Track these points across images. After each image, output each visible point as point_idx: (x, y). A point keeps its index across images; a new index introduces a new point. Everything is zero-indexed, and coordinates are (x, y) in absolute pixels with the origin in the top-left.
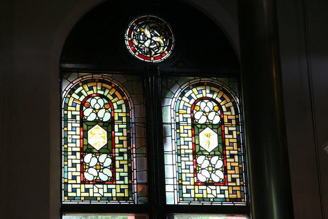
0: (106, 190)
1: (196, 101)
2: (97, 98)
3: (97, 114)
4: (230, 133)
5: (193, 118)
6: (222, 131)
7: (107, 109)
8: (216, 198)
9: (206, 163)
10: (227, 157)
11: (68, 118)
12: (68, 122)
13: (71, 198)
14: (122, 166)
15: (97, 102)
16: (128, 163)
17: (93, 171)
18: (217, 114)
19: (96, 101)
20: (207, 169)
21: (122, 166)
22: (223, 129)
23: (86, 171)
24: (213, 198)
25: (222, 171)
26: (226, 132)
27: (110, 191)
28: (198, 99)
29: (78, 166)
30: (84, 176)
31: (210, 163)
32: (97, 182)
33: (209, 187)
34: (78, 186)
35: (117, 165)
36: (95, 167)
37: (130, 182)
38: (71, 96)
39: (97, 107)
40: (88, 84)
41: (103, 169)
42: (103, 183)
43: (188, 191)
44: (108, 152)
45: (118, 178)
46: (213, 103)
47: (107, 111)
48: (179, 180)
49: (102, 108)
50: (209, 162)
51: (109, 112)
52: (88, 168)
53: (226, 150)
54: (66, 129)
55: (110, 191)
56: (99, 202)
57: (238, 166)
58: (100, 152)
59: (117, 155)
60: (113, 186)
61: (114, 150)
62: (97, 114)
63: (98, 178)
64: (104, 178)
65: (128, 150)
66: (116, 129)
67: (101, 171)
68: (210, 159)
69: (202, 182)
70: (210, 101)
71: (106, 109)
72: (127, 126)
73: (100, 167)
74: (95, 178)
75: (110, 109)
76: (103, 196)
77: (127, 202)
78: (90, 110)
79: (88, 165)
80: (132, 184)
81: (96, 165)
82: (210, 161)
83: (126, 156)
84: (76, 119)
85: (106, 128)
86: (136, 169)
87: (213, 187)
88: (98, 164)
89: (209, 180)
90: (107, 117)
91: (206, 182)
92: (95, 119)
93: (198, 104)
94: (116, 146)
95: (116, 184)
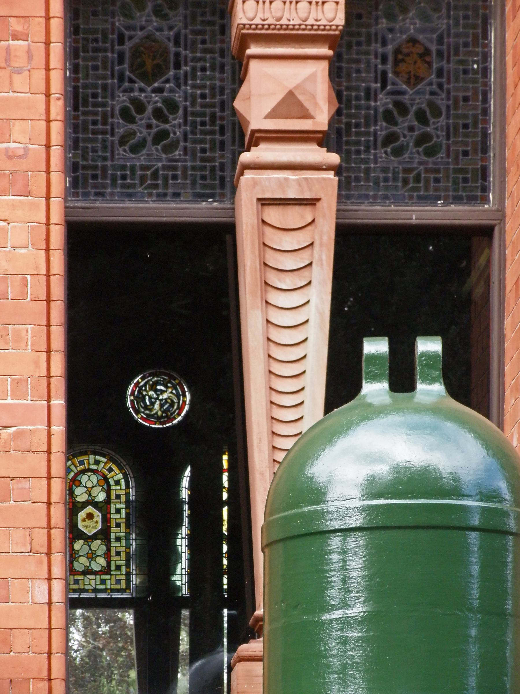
1: (76, 474)
4: (118, 511)
10: (112, 540)
15: (89, 479)
17: (83, 560)
21: (118, 553)
27: (103, 582)
28: (79, 472)
32: (87, 572)
35: (113, 553)
36: (86, 556)
42: (95, 573)
43: (118, 582)
50: (92, 547)
55: (103, 582)
58: (94, 537)
60: (108, 577)
64: (95, 567)
66: (113, 511)
67: (94, 559)
68: (90, 543)
73: (92, 556)
74: (86, 568)
75: (105, 487)
82: (89, 546)
83: (124, 542)
87: (92, 577)
88: (90, 552)
90: (101, 497)
91: (84, 571)
92: (87, 500)
93: (78, 478)
95: (111, 575)
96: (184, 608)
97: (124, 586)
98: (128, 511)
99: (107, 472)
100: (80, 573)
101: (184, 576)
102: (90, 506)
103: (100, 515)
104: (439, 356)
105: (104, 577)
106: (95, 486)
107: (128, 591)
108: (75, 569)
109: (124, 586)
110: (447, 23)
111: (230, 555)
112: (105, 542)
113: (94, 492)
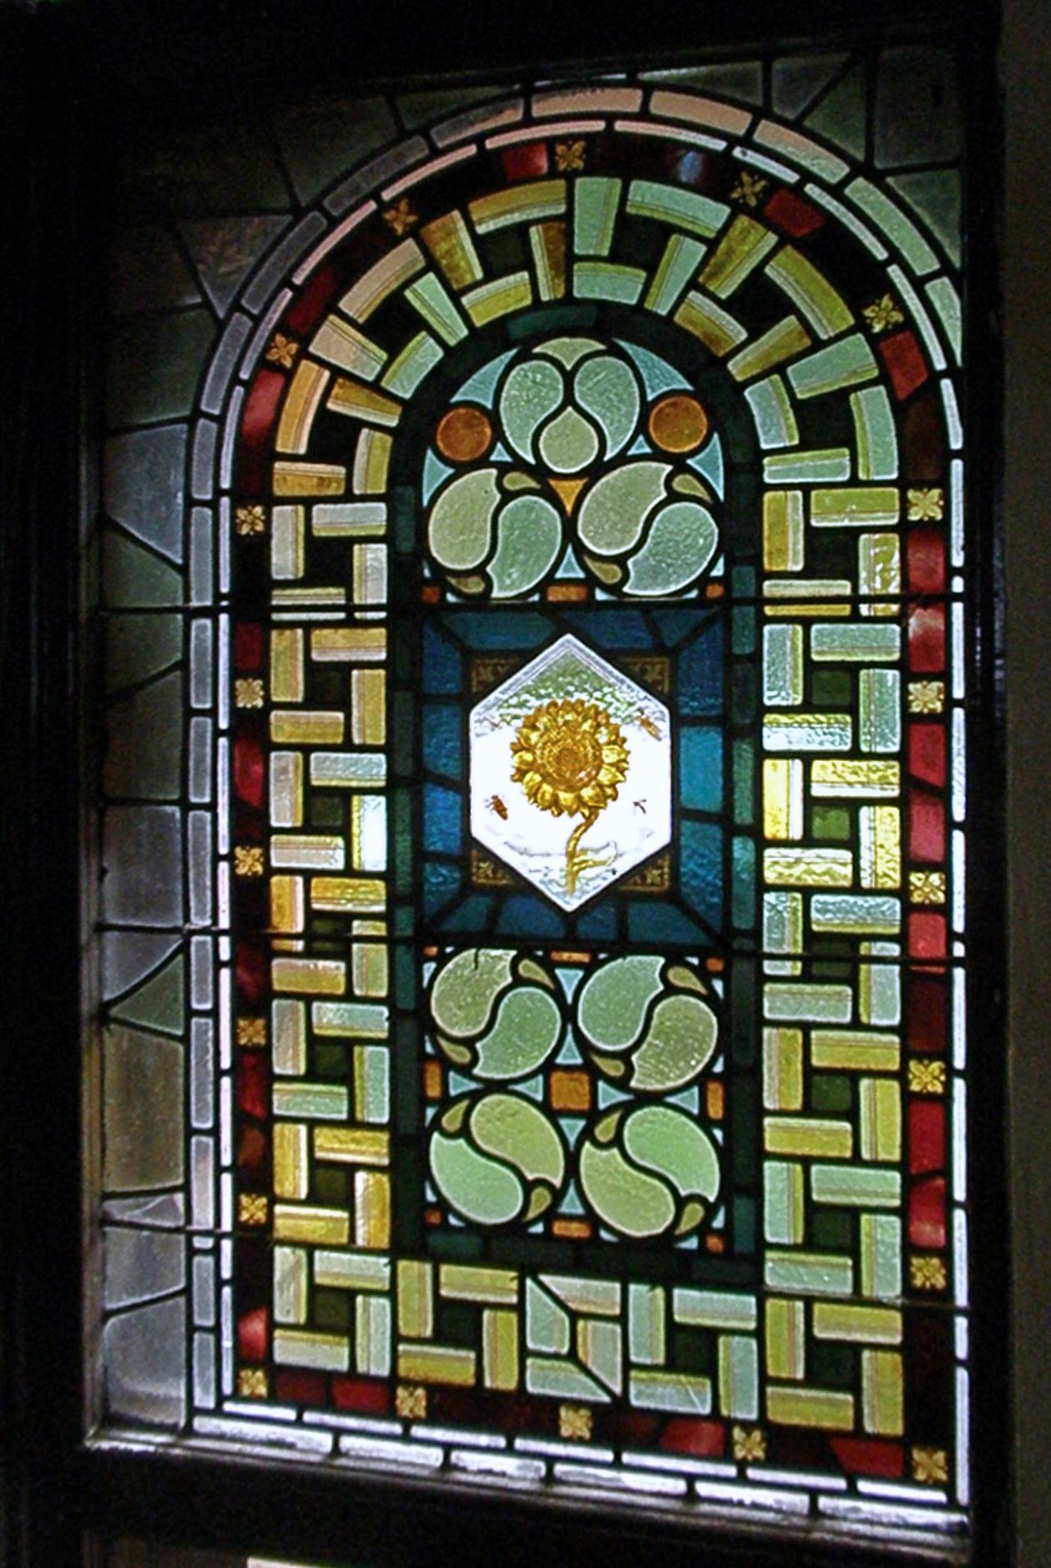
9: (360, 1020)
15: (569, 400)
18: (681, 484)
22: (743, 648)
23: (451, 1120)
25: (704, 1121)
38: (303, 354)
40: (477, 209)
44: (689, 934)
52: (627, 1109)
54: (926, 696)
69: (472, 1226)
75: (712, 465)
79: (614, 1069)
81: (548, 1068)
85: (657, 669)
87: (600, 1293)
89: (550, 1215)
91: (517, 1226)
93: (475, 389)
95: (754, 1285)
96: (476, 197)
99: (794, 944)
102: (569, 637)
103: (666, 712)
104: (339, 724)
106: (622, 459)
107: (927, 1461)
108: (443, 1206)
110: (871, 327)
111: (975, 653)
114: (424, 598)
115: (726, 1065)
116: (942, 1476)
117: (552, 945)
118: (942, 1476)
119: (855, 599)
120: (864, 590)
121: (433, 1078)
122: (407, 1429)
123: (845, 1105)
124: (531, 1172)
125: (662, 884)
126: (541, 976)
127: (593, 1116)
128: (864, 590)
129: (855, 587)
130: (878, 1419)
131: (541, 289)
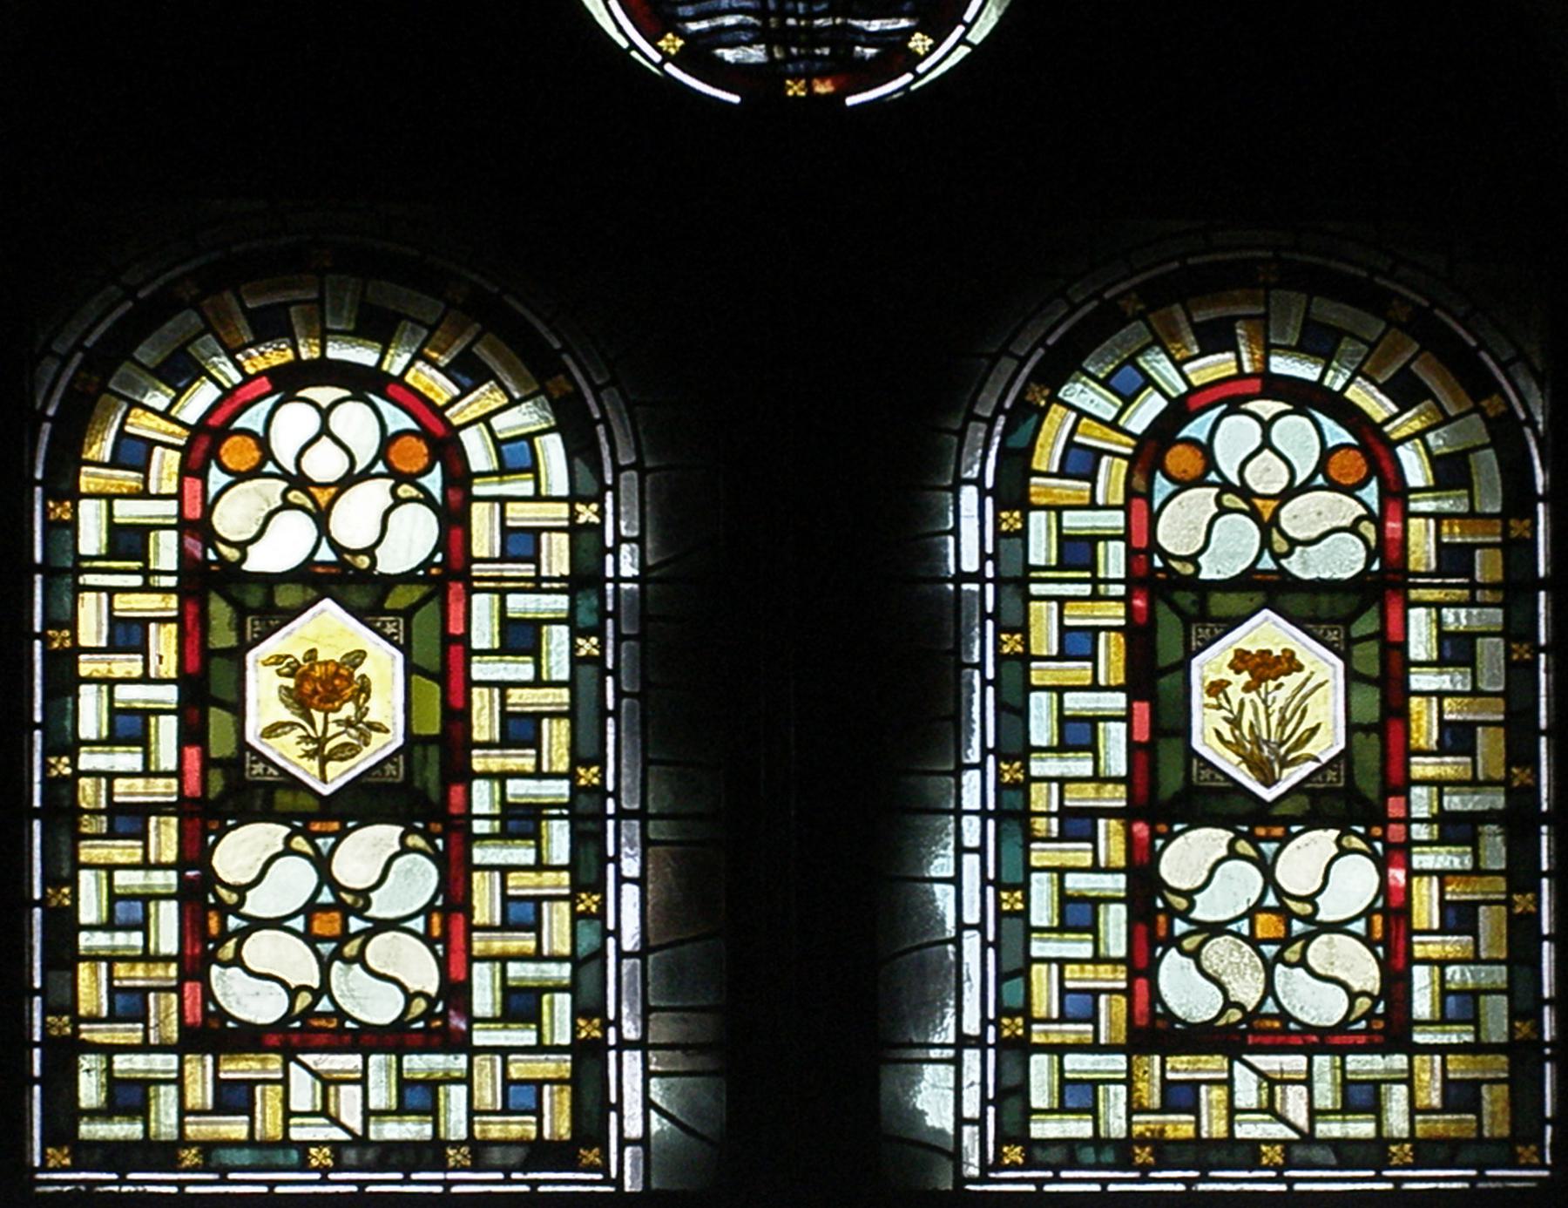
0: (1326, 1095)
2: (1267, 408)
3: (321, 518)
5: (1143, 550)
6: (447, 639)
7: (411, 479)
8: (1308, 1138)
11: (1033, 560)
12: (1414, 594)
13: (1055, 1155)
14: (1458, 918)
16: (577, 887)
19: (312, 421)
20: (298, 924)
24: (1286, 1144)
26: (484, 633)
29: (1115, 921)
30: (208, 995)
31: (1270, 880)
33: (308, 1059)
34: (164, 1063)
35: (485, 903)
37: (589, 1030)
39: (325, 464)
41: (368, 935)
45: (485, 999)
46: (385, 407)
47: (406, 490)
48: (1001, 1010)
49: (366, 475)
50: (1281, 875)
51: (428, 500)
53: (470, 776)
56: (324, 1181)
57: (1509, 903)
59: (1420, 832)
61: (457, 792)
62: (321, 518)
63: (324, 1005)
65: (574, 789)
67: (351, 949)
68: (1269, 848)
70: (1299, 410)
71: (399, 477)
72: (1507, 618)
74: (304, 1000)
75: (434, 482)
76: (1308, 1138)
77: (1378, 1178)
78: (1202, 500)
80: (600, 1047)
83: (559, 839)
84: (1093, 567)
86: (981, 927)
92: (310, 560)
94: (1422, 768)
95: (1413, 1050)
97: (558, 1122)
98: (587, 646)
100: (973, 1042)
101: (971, 1057)
105: (1362, 1064)
106: (1307, 487)
109: (558, 1122)
112: (428, 836)
113: (1299, 517)
114: (80, 1136)
115: (444, 900)
116: (51, 1164)
117: (307, 817)
118: (51, 1164)
119: (538, 579)
120: (544, 573)
121: (97, 1131)
122: (991, 1022)
123: (1068, 651)
124: (379, 898)
125: (397, 776)
126: (231, 944)
127: (345, 937)
128: (544, 573)
129: (538, 570)
130: (1425, 1126)
131: (309, 297)
